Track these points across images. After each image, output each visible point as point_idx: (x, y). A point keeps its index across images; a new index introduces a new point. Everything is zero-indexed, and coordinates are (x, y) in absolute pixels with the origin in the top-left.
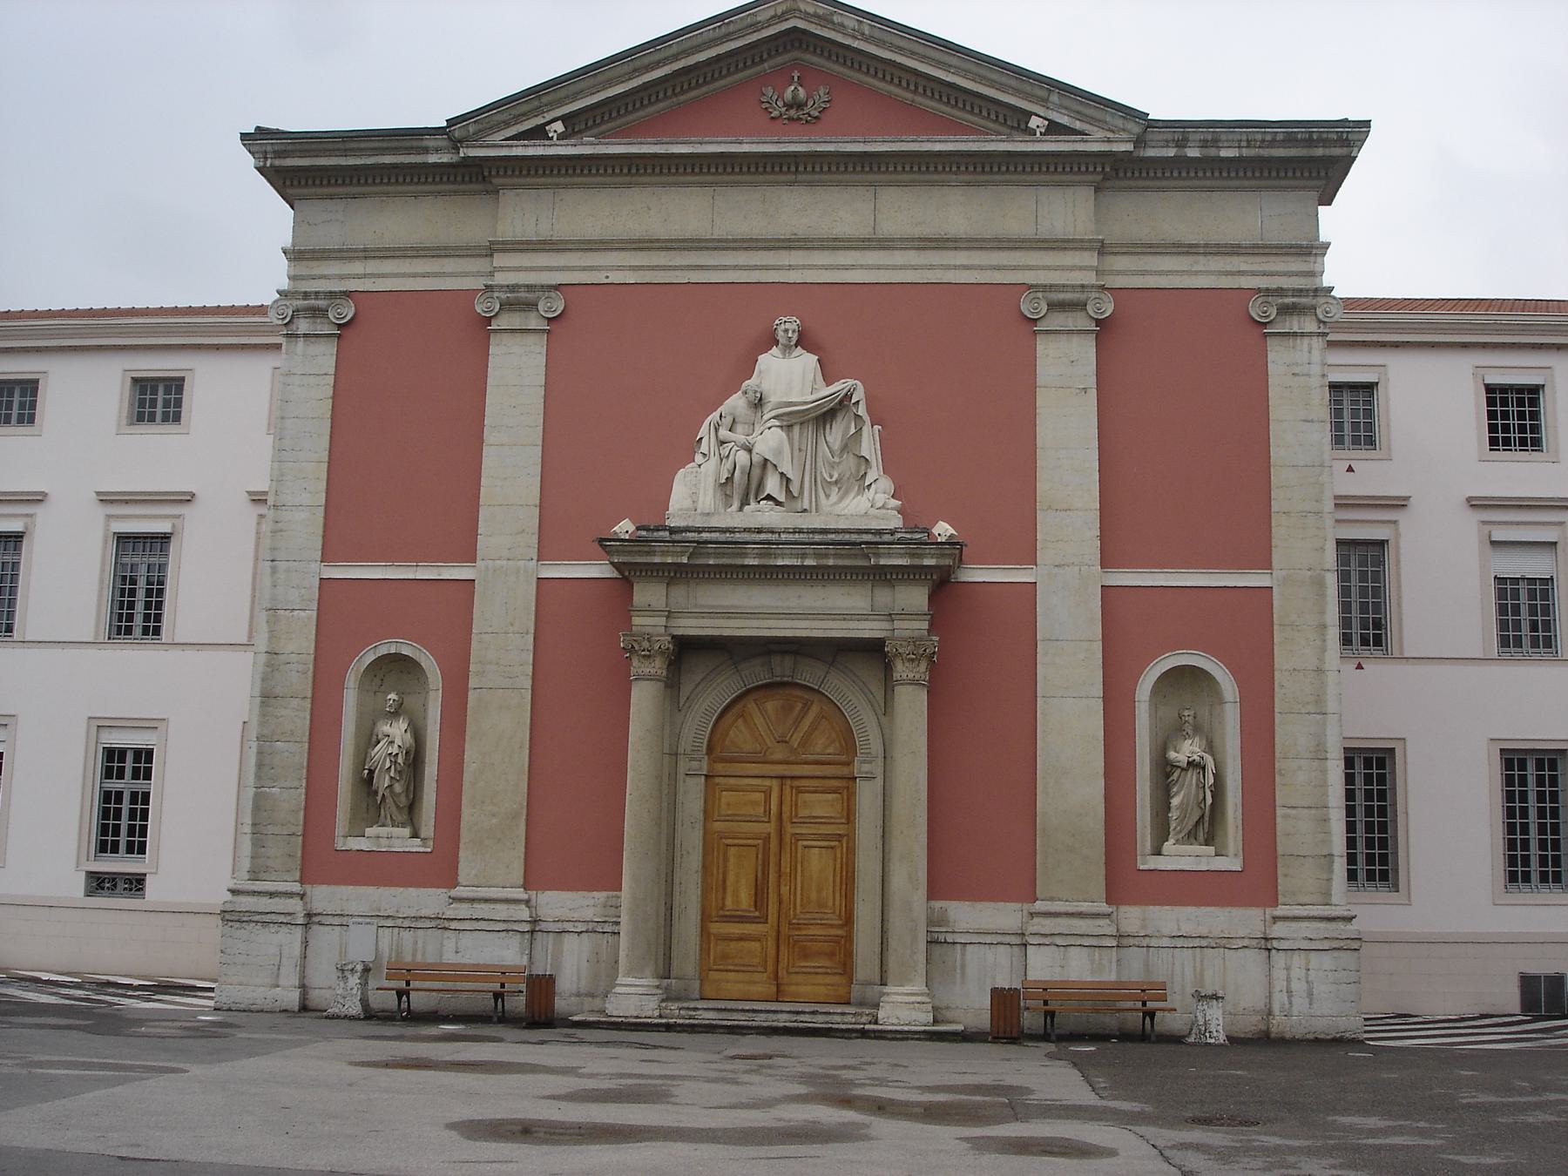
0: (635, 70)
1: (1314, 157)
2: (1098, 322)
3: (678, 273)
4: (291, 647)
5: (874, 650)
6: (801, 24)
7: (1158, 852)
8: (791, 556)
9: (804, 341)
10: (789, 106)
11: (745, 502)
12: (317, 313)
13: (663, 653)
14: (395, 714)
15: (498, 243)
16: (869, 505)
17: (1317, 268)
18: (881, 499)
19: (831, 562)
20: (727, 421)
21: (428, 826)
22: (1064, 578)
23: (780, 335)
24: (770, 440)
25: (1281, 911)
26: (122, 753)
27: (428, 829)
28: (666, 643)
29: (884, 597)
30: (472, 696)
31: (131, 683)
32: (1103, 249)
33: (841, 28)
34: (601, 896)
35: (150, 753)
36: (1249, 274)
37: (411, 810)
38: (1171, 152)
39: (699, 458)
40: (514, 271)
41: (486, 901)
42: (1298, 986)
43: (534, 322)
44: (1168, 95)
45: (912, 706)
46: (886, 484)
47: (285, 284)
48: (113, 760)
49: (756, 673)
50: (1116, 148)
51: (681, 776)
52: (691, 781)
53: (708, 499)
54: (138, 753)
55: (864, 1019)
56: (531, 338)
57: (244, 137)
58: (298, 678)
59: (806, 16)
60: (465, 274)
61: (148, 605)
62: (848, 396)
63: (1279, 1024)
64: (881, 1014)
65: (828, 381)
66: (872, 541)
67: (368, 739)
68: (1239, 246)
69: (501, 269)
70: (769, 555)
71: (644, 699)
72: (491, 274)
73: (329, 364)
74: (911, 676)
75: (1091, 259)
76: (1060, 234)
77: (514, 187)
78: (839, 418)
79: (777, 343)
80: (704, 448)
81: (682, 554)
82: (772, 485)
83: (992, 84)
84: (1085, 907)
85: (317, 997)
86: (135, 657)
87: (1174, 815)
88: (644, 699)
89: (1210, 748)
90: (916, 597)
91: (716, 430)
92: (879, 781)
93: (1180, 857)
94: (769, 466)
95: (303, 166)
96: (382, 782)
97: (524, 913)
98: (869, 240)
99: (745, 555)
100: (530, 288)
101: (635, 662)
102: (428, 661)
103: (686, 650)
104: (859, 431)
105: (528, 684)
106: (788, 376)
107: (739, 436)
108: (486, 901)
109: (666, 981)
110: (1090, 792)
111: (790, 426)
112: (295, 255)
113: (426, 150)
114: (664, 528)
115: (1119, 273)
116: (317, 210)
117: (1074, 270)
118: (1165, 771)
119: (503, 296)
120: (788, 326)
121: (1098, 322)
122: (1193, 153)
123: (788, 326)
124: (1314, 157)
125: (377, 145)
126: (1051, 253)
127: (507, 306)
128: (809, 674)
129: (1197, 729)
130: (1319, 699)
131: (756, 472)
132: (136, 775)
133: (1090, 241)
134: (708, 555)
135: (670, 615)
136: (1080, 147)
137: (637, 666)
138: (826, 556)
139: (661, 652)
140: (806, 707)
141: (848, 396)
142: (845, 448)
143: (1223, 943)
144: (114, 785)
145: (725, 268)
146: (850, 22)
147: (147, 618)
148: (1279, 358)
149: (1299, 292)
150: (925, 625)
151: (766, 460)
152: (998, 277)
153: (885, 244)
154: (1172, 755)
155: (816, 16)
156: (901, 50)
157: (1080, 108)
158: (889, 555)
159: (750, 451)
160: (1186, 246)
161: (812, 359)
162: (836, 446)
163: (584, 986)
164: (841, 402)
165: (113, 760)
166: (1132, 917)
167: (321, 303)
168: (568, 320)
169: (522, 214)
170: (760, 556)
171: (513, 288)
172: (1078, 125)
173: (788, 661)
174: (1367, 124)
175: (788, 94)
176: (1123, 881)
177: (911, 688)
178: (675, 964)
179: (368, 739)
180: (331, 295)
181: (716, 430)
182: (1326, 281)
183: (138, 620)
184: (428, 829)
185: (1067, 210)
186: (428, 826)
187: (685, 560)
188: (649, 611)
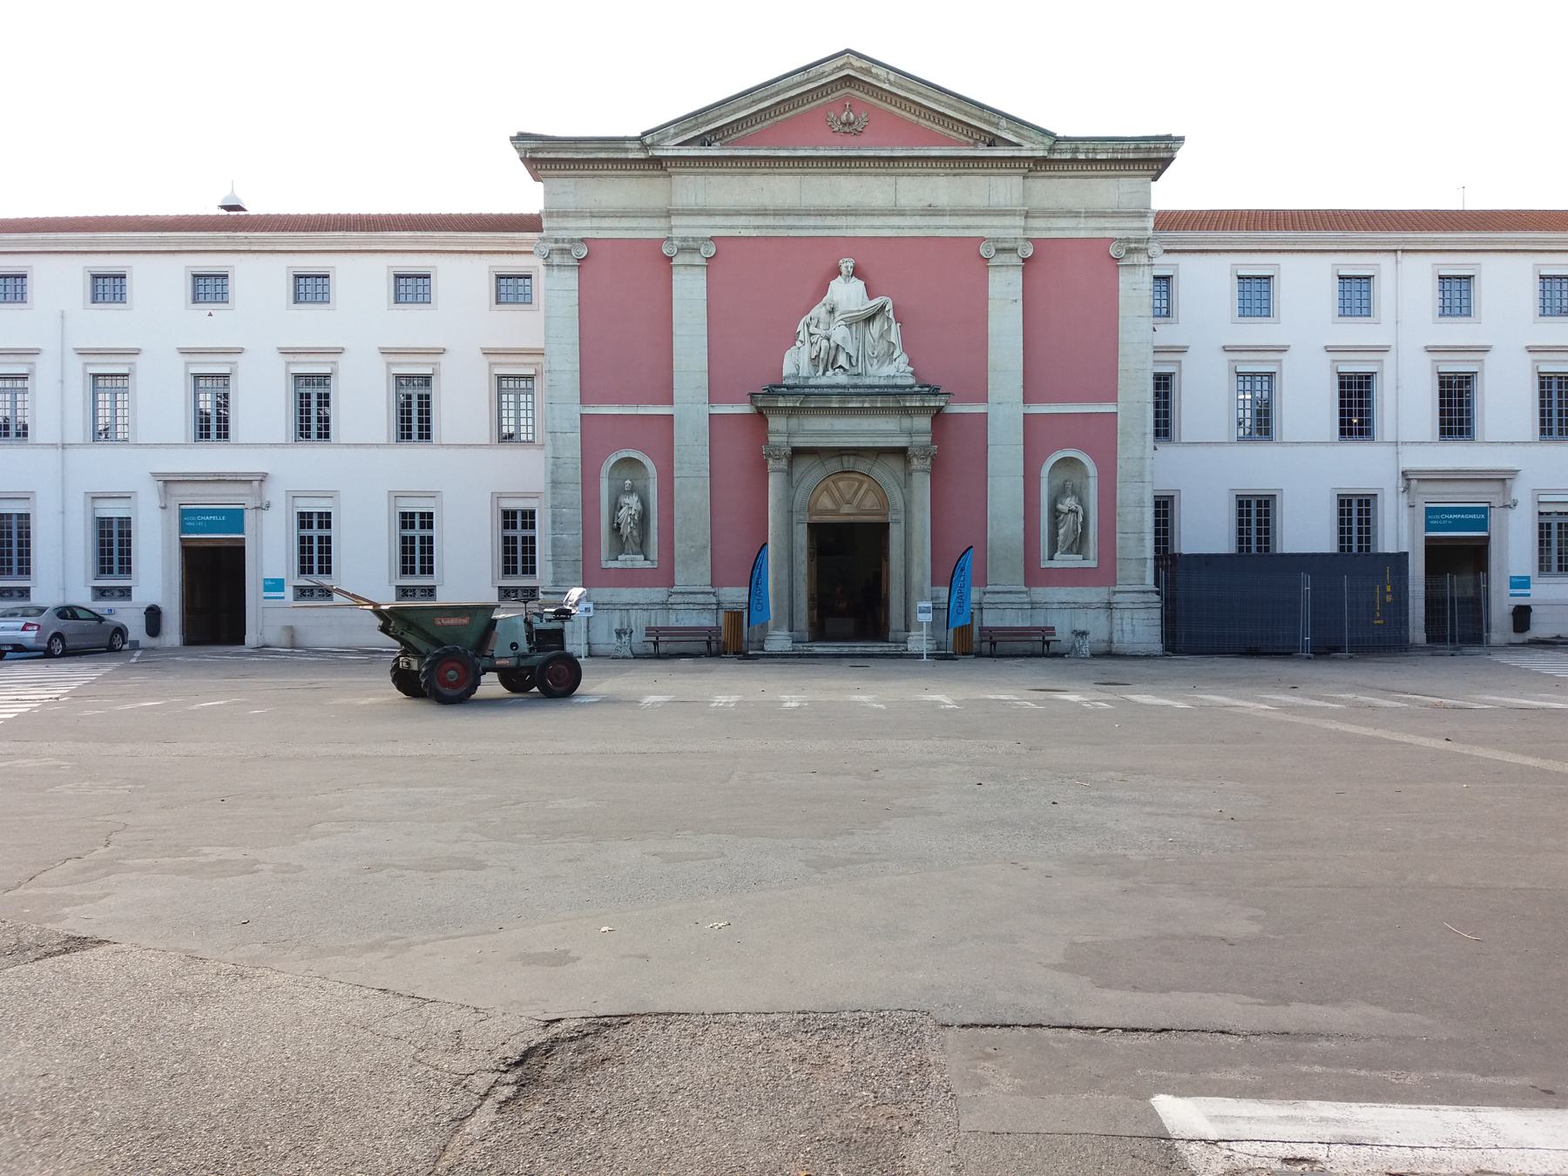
1: (1153, 156)
4: (568, 455)
5: (901, 452)
6: (852, 73)
7: (1051, 558)
9: (857, 273)
10: (844, 124)
14: (631, 491)
16: (897, 370)
18: (903, 367)
21: (654, 552)
22: (1004, 407)
24: (839, 334)
25: (1117, 588)
26: (514, 513)
27: (654, 555)
28: (788, 451)
29: (906, 423)
31: (414, 470)
32: (1027, 215)
33: (876, 77)
35: (532, 513)
37: (642, 547)
39: (798, 344)
40: (685, 228)
42: (1127, 628)
43: (698, 260)
44: (1066, 125)
45: (922, 486)
46: (904, 358)
48: (407, 519)
49: (834, 465)
50: (1037, 154)
53: (805, 370)
54: (524, 513)
56: (697, 270)
57: (512, 139)
58: (573, 471)
59: (853, 68)
60: (653, 229)
61: (420, 420)
62: (883, 307)
63: (1115, 648)
65: (871, 297)
66: (898, 392)
67: (616, 507)
71: (775, 483)
72: (670, 228)
73: (574, 284)
75: (1020, 221)
77: (679, 174)
82: (842, 360)
85: (597, 649)
86: (414, 452)
87: (1061, 538)
89: (1081, 502)
90: (924, 423)
93: (1064, 561)
95: (543, 156)
96: (626, 530)
97: (714, 600)
102: (648, 463)
106: (847, 294)
107: (821, 331)
110: (1016, 529)
113: (626, 150)
115: (1037, 229)
116: (557, 184)
117: (1010, 229)
118: (1055, 514)
120: (847, 265)
122: (1082, 156)
124: (1153, 156)
127: (681, 250)
128: (862, 465)
129: (1073, 493)
130: (1141, 474)
131: (832, 353)
132: (524, 526)
136: (1017, 154)
140: (861, 483)
141: (883, 307)
142: (881, 336)
143: (1086, 606)
144: (306, 532)
145: (809, 227)
147: (420, 428)
148: (1126, 280)
149: (1138, 241)
152: (967, 233)
153: (901, 213)
154: (1060, 506)
160: (1078, 207)
161: (861, 284)
162: (876, 336)
165: (407, 519)
166: (1041, 593)
167: (567, 246)
169: (690, 189)
171: (684, 239)
172: (1015, 140)
173: (852, 459)
174: (1182, 139)
175: (844, 118)
176: (1033, 575)
179: (616, 507)
180: (572, 241)
183: (415, 431)
184: (654, 555)
186: (654, 552)
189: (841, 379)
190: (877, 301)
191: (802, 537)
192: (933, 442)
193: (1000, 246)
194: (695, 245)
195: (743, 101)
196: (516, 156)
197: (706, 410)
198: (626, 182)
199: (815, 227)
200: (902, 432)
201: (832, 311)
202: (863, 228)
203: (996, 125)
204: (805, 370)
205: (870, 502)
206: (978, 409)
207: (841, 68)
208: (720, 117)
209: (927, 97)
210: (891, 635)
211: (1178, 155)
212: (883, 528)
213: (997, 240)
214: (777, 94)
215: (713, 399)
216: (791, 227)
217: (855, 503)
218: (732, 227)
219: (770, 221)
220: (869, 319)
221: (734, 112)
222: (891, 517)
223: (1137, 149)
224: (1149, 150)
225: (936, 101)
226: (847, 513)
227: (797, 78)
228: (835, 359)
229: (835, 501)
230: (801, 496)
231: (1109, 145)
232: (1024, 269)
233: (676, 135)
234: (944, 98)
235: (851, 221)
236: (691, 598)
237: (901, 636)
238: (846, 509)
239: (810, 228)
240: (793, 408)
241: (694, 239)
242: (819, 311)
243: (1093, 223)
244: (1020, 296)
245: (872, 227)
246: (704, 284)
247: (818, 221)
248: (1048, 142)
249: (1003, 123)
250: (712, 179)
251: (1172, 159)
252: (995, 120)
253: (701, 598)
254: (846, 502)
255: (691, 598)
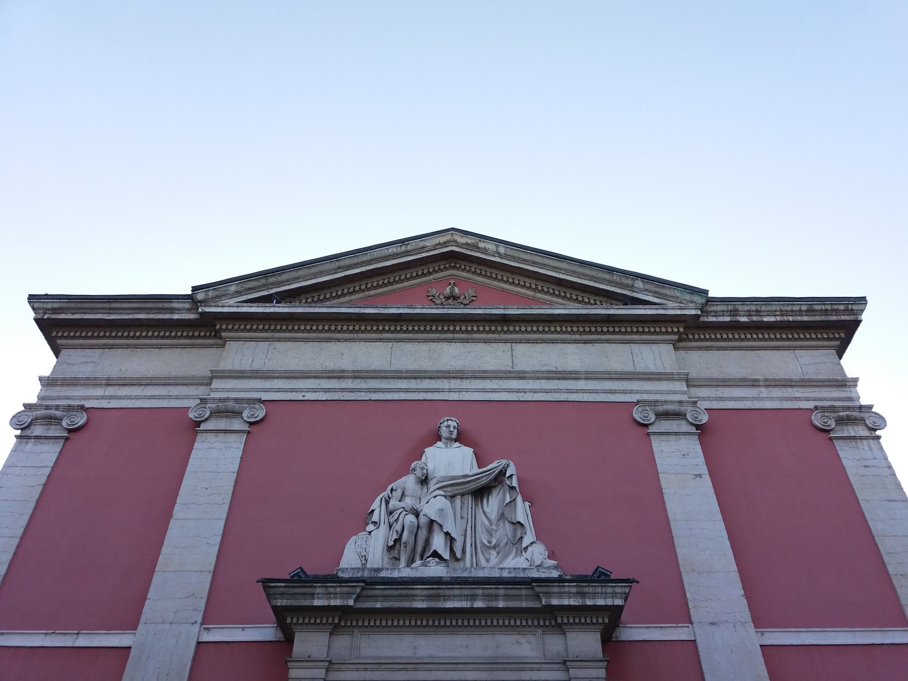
0: (339, 268)
2: (698, 427)
9: (461, 438)
10: (447, 298)
12: (51, 420)
15: (218, 371)
16: (534, 558)
17: (853, 395)
19: (501, 604)
20: (398, 493)
23: (444, 432)
24: (435, 505)
29: (554, 644)
33: (485, 251)
36: (803, 399)
38: (727, 319)
39: (370, 527)
40: (223, 389)
43: (237, 425)
47: (33, 400)
56: (232, 437)
62: (502, 473)
68: (791, 380)
69: (217, 390)
75: (681, 386)
76: (652, 368)
78: (495, 493)
79: (439, 438)
80: (375, 517)
81: (349, 595)
83: (592, 278)
91: (387, 503)
94: (436, 526)
98: (510, 372)
99: (412, 597)
100: (236, 400)
107: (408, 502)
111: (453, 496)
112: (46, 382)
113: (173, 310)
120: (449, 426)
123: (450, 423)
125: (136, 305)
127: (217, 413)
131: (423, 534)
134: (375, 598)
141: (502, 473)
142: (502, 516)
146: (491, 247)
153: (521, 375)
155: (467, 244)
156: (525, 261)
157: (657, 290)
158: (561, 595)
159: (417, 515)
161: (470, 451)
162: (494, 515)
167: (58, 413)
168: (265, 426)
169: (242, 354)
170: (429, 597)
181: (387, 503)
182: (864, 401)
185: (656, 355)
187: (351, 602)
189: (435, 570)
193: (660, 408)
194: (237, 407)
195: (328, 266)
196: (32, 315)
197: (192, 633)
198: (166, 353)
199: (407, 391)
201: (424, 481)
202: (473, 390)
203: (631, 288)
206: (680, 634)
207: (445, 244)
208: (297, 279)
209: (543, 266)
211: (864, 317)
213: (656, 403)
214: (369, 262)
216: (376, 390)
218: (292, 390)
220: (481, 493)
221: (315, 275)
223: (810, 311)
224: (826, 312)
225: (554, 269)
227: (393, 250)
228: (427, 542)
231: (775, 307)
232: (700, 436)
233: (238, 293)
234: (564, 265)
239: (400, 391)
240: (343, 610)
242: (409, 481)
243: (778, 392)
246: (239, 453)
247: (413, 384)
248: (700, 300)
249: (639, 284)
250: (278, 345)
251: (858, 322)
252: (629, 282)
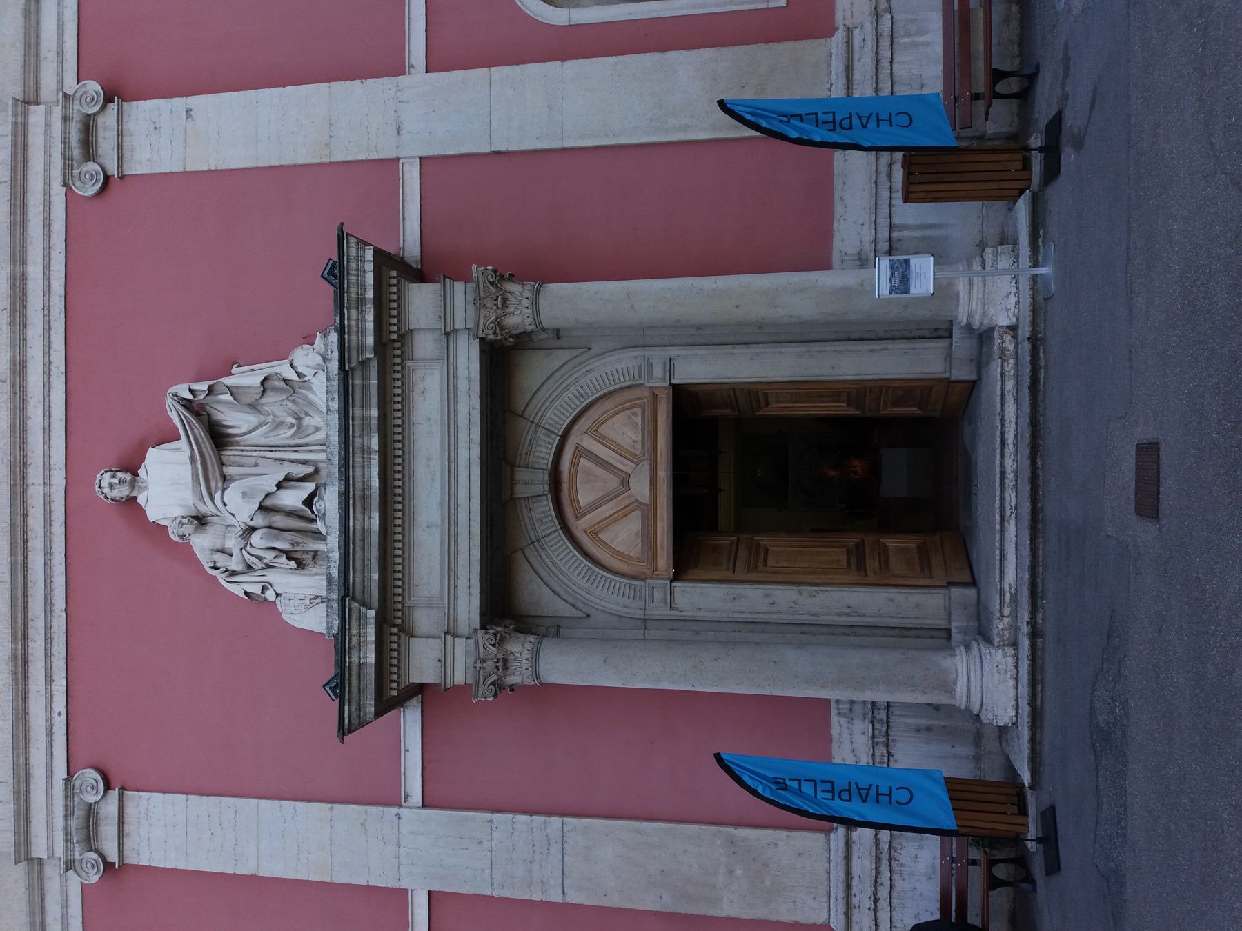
2: (108, 100)
3: (55, 623)
8: (365, 467)
9: (132, 465)
11: (318, 536)
13: (502, 640)
15: (17, 852)
20: (221, 559)
23: (121, 492)
24: (238, 504)
29: (425, 345)
30: (574, 898)
34: (837, 724)
39: (270, 595)
41: (848, 887)
43: (110, 808)
45: (569, 301)
51: (674, 614)
52: (680, 599)
55: (1010, 346)
56: (130, 811)
62: (187, 404)
64: (1003, 320)
69: (51, 848)
70: (365, 498)
71: (563, 666)
74: (526, 303)
75: (37, 115)
78: (218, 416)
80: (256, 589)
81: (362, 618)
84: (838, 65)
88: (563, 666)
90: (422, 301)
91: (234, 573)
92: (674, 352)
94: (268, 503)
98: (12, 386)
99: (366, 532)
101: (514, 679)
103: (502, 607)
104: (230, 390)
105: (556, 821)
108: (848, 887)
109: (956, 636)
111: (224, 478)
114: (341, 642)
119: (77, 848)
120: (109, 485)
121: (108, 100)
126: (30, 163)
127: (90, 840)
131: (280, 521)
133: (15, 115)
135: (450, 633)
137: (519, 676)
138: (365, 419)
139: (500, 641)
140: (580, 452)
141: (187, 404)
142: (254, 407)
145: (48, 565)
150: (459, 287)
151: (262, 508)
158: (361, 332)
161: (152, 454)
163: (966, 750)
164: (197, 414)
170: (366, 509)
177: (542, 302)
178: (929, 622)
181: (234, 573)
188: (444, 661)
189: (329, 502)
190: (175, 414)
191: (704, 597)
192: (466, 279)
193: (77, 153)
194: (79, 813)
199: (48, 552)
200: (448, 357)
201: (201, 521)
204: (313, 583)
205: (625, 430)
206: (411, 176)
210: (962, 373)
212: (686, 401)
215: (392, 798)
217: (627, 467)
218: (49, 733)
219: (37, 648)
220: (219, 437)
222: (658, 378)
226: (650, 485)
228: (291, 513)
229: (624, 513)
230: (609, 598)
232: (123, 99)
235: (35, 476)
236: (862, 889)
237: (961, 345)
238: (640, 488)
241: (67, 816)
242: (201, 543)
244: (179, 103)
245: (47, 430)
246: (157, 796)
247: (36, 545)
253: (862, 865)
254: (619, 481)
255: (862, 889)
